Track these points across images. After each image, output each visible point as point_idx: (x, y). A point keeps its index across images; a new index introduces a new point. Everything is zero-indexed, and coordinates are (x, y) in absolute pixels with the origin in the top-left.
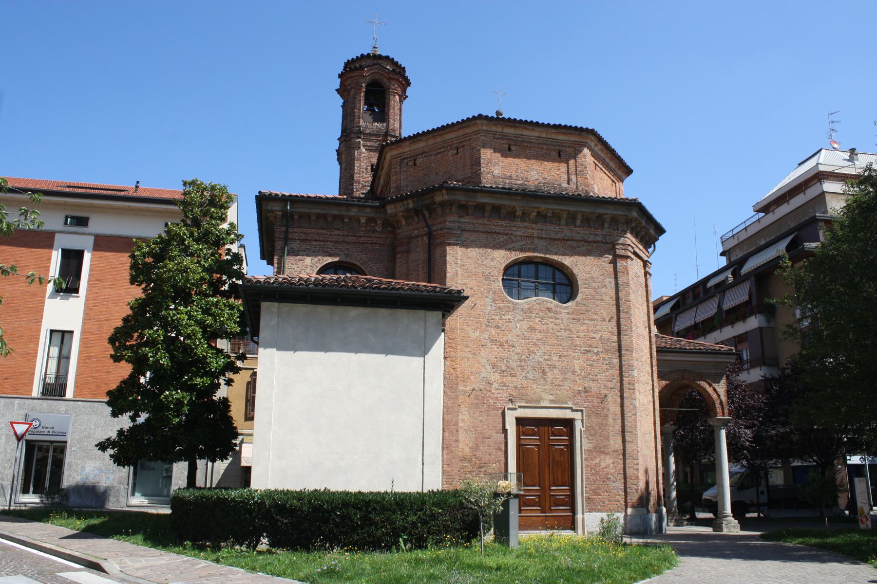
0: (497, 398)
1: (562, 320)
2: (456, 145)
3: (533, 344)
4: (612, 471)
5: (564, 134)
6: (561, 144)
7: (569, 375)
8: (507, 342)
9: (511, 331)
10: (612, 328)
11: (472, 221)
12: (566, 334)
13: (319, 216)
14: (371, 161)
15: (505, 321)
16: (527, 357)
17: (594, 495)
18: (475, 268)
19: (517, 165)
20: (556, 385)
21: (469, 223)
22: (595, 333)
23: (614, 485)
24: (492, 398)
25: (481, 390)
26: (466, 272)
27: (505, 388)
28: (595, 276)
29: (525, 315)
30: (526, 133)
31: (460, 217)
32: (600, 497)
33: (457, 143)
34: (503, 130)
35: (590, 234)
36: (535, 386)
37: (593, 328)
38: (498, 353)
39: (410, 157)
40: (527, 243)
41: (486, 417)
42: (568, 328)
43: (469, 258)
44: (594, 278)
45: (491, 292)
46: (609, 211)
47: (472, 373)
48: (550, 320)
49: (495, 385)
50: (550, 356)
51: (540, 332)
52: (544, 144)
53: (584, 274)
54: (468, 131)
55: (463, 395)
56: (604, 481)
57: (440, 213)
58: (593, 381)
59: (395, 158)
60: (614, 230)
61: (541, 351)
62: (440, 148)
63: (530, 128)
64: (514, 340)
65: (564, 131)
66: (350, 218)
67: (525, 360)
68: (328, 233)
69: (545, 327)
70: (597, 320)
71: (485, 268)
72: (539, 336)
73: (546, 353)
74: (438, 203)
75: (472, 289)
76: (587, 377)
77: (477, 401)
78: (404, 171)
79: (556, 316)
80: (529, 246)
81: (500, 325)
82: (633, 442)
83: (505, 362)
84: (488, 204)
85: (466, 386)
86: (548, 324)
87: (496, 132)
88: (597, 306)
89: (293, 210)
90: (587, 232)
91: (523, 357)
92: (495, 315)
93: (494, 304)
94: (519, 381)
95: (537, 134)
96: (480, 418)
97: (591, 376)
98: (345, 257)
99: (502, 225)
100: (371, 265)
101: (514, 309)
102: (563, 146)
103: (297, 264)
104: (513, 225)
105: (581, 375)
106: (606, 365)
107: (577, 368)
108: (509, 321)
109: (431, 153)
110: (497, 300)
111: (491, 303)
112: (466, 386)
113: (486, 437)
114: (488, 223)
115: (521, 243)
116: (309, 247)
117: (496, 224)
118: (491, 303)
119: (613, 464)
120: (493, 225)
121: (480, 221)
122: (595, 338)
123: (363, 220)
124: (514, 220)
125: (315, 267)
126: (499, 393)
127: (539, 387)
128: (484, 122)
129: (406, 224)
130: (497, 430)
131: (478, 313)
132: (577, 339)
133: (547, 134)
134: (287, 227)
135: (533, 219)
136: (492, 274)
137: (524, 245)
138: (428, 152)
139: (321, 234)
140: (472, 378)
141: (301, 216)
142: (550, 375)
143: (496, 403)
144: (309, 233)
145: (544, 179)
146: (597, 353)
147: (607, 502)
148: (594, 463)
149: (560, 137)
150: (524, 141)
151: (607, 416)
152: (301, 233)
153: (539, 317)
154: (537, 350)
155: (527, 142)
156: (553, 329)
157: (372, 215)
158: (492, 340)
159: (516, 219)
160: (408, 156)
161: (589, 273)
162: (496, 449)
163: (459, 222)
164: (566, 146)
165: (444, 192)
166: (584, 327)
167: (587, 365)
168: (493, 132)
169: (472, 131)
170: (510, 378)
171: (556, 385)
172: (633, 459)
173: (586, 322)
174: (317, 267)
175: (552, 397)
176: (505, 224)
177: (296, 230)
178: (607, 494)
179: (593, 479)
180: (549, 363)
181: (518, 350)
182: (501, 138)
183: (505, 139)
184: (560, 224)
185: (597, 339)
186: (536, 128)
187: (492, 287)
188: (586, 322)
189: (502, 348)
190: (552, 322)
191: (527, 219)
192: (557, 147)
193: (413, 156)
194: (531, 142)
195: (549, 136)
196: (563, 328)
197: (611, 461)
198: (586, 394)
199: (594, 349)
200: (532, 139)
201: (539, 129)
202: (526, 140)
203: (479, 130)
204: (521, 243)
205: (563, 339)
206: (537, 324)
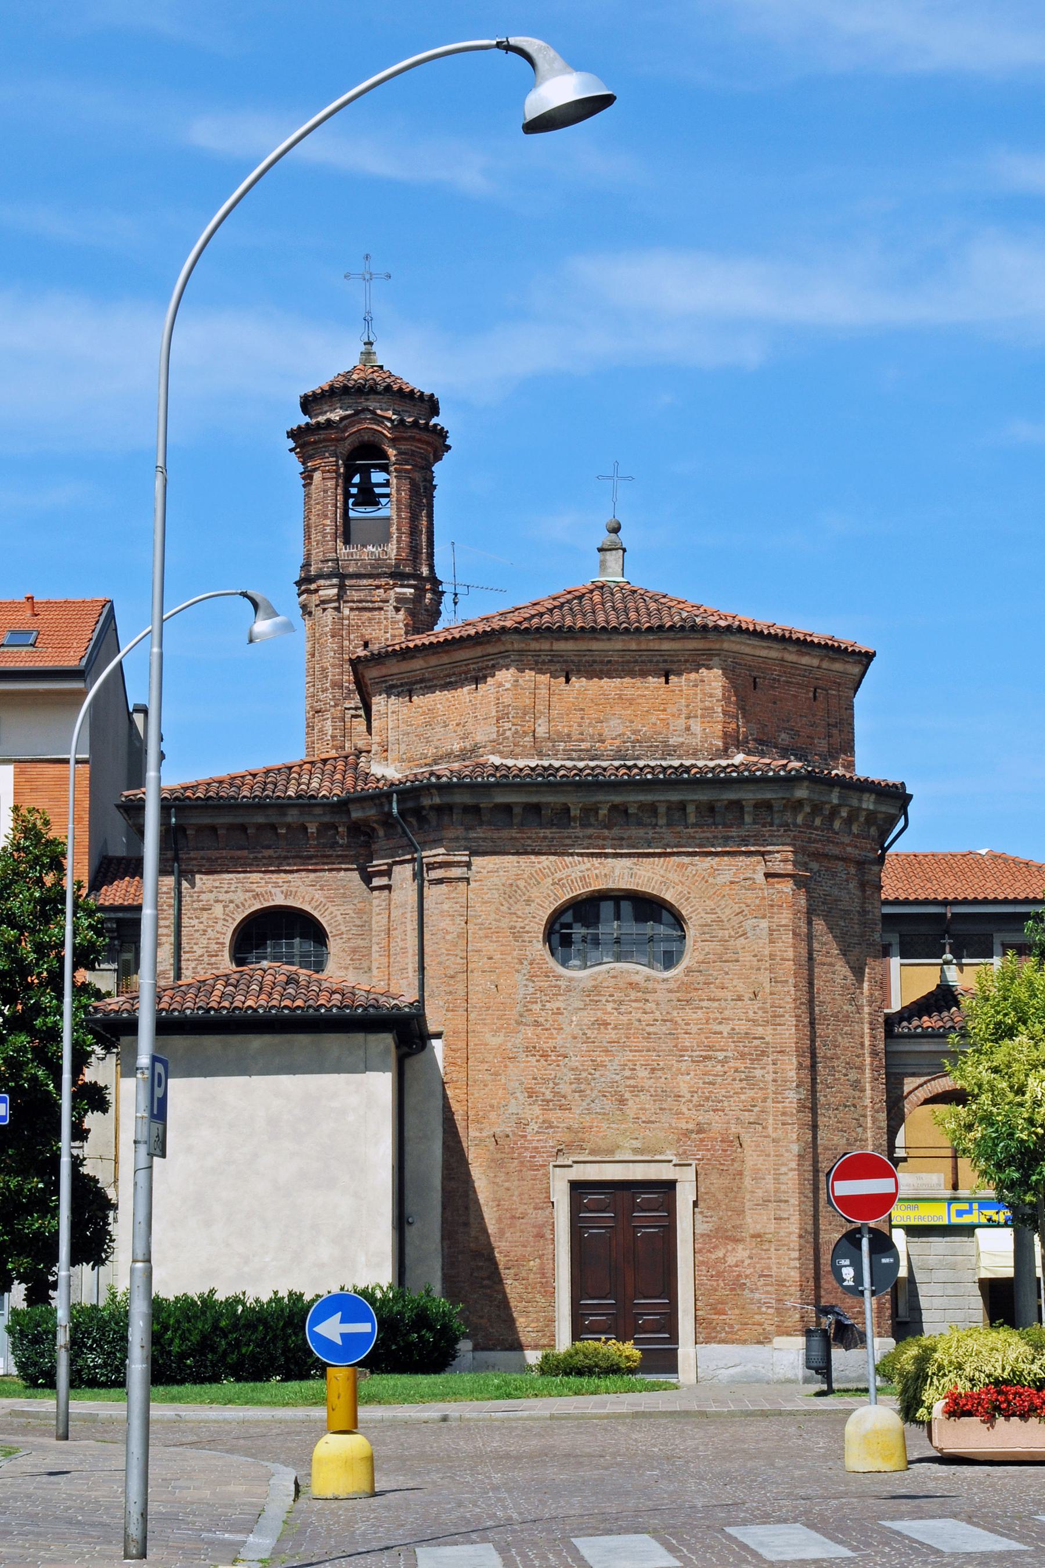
0: (536, 1148)
1: (658, 1004)
2: (473, 674)
3: (603, 1051)
4: (748, 1272)
5: (673, 639)
6: (669, 658)
7: (669, 1102)
8: (554, 1049)
9: (562, 1029)
10: (755, 1013)
11: (489, 834)
12: (664, 1028)
13: (231, 827)
14: (362, 636)
15: (550, 1012)
16: (590, 1074)
17: (715, 1314)
18: (495, 920)
19: (583, 710)
20: (644, 1122)
21: (484, 839)
22: (720, 1023)
23: (751, 1295)
24: (526, 1149)
25: (508, 1136)
26: (480, 929)
27: (551, 1131)
28: (723, 917)
29: (588, 999)
30: (595, 645)
31: (468, 828)
32: (724, 1317)
33: (474, 669)
34: (552, 646)
35: (715, 837)
36: (605, 1125)
37: (718, 1015)
38: (539, 1070)
39: (402, 685)
40: (593, 865)
41: (516, 1183)
42: (669, 1017)
43: (486, 903)
44: (722, 921)
45: (525, 963)
46: (749, 795)
47: (492, 1106)
48: (634, 1005)
49: (534, 1126)
50: (635, 1069)
51: (615, 1028)
52: (636, 662)
53: (703, 915)
54: (491, 649)
55: (476, 1145)
56: (732, 1290)
57: (434, 823)
58: (714, 1111)
59: (377, 683)
60: (764, 826)
61: (617, 1062)
62: (449, 676)
63: (604, 637)
64: (568, 1045)
65: (671, 635)
66: (289, 826)
67: (586, 1079)
68: (251, 856)
69: (624, 1018)
70: (726, 1000)
71: (515, 919)
72: (613, 1035)
73: (626, 1065)
74: (427, 807)
75: (491, 958)
76: (703, 1106)
77: (499, 1156)
78: (393, 712)
79: (648, 996)
80: (597, 871)
81: (541, 1020)
82: (788, 1219)
83: (551, 1085)
84: (517, 803)
85: (481, 1130)
86: (631, 1013)
87: (540, 651)
88: (727, 973)
89: (181, 822)
90: (709, 835)
91: (584, 1075)
92: (533, 1003)
93: (531, 984)
94: (574, 1117)
95: (619, 646)
96: (506, 1184)
97: (711, 1103)
98: (283, 897)
99: (545, 838)
100: (332, 909)
101: (568, 990)
102: (672, 662)
103: (197, 918)
104: (566, 835)
105: (691, 1101)
106: (741, 1080)
107: (684, 1090)
108: (558, 1012)
109: (435, 682)
110: (537, 976)
111: (525, 982)
112: (481, 1130)
113: (517, 1215)
114: (518, 835)
115: (583, 867)
116: (217, 884)
117: (534, 836)
118: (525, 982)
119: (751, 1258)
120: (529, 838)
121: (505, 833)
122: (721, 1033)
123: (312, 829)
124: (567, 826)
125: (230, 921)
126: (541, 1140)
127: (612, 1125)
128: (516, 637)
129: (385, 836)
130: (537, 1204)
131: (503, 1000)
132: (687, 1036)
133: (639, 644)
134: (176, 851)
135: (603, 821)
136: (527, 928)
137: (588, 870)
138: (430, 680)
139: (239, 858)
140: (493, 1116)
141: (200, 829)
142: (632, 1107)
143: (534, 1157)
144: (217, 859)
145: (635, 732)
146: (724, 1062)
147: (737, 1327)
148: (713, 1257)
149: (666, 646)
150: (595, 662)
151: (741, 1173)
152: (203, 858)
153: (614, 1001)
154: (610, 1061)
155: (602, 662)
156: (639, 1021)
157: (326, 819)
158: (527, 1048)
159: (572, 824)
160: (399, 682)
161: (713, 912)
162: (536, 1236)
163: (466, 839)
164: (680, 661)
165: (434, 791)
166: (700, 1014)
167: (704, 1083)
168: (535, 651)
169: (496, 650)
170: (559, 1113)
171: (644, 1122)
172: (788, 1250)
173: (705, 1004)
174: (234, 920)
175: (637, 1144)
176: (550, 836)
177: (192, 854)
178: (737, 1311)
179: (712, 1286)
180: (632, 1082)
181: (575, 1062)
182: (551, 661)
183: (559, 662)
184: (656, 825)
185: (725, 1034)
186: (614, 637)
187: (528, 953)
188: (705, 1004)
189: (546, 1061)
190: (638, 1008)
191: (592, 820)
192: (661, 666)
193: (406, 684)
194: (609, 662)
195: (643, 647)
196: (660, 1018)
197: (746, 1254)
198: (701, 1136)
199: (719, 1053)
200: (612, 656)
201: (620, 637)
202: (598, 659)
203: (507, 651)
204: (583, 867)
205: (660, 1038)
206: (610, 1013)
